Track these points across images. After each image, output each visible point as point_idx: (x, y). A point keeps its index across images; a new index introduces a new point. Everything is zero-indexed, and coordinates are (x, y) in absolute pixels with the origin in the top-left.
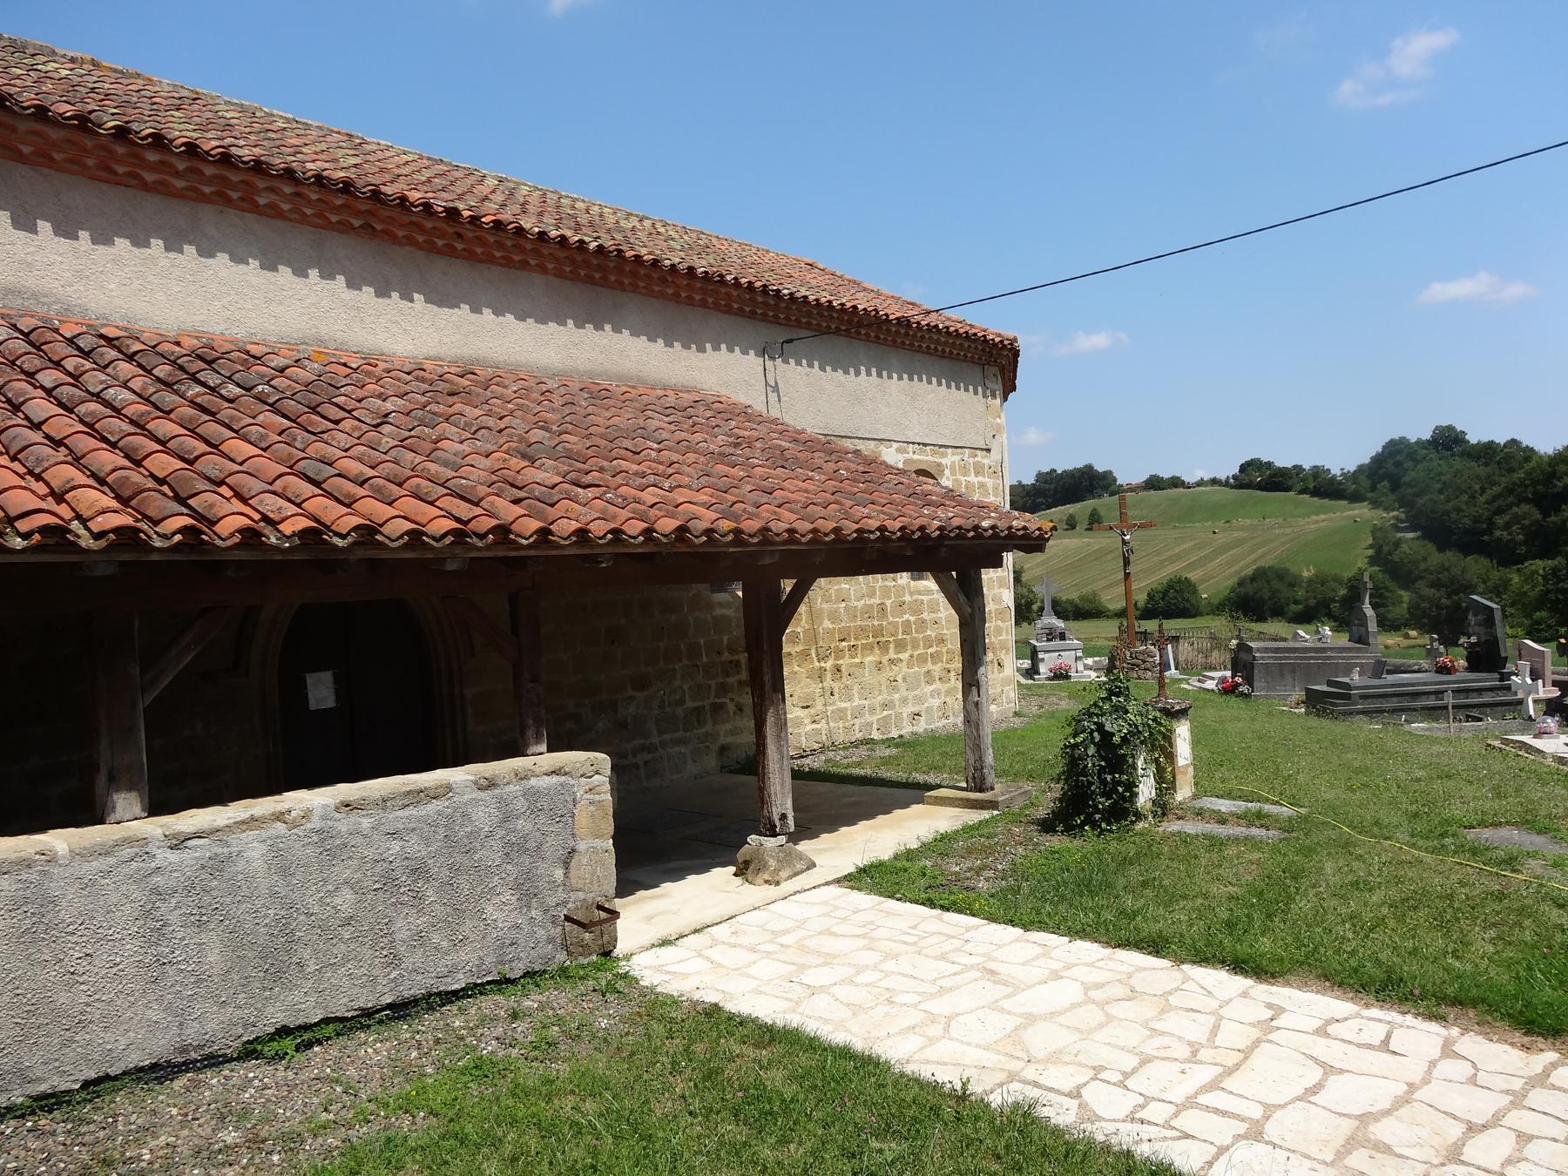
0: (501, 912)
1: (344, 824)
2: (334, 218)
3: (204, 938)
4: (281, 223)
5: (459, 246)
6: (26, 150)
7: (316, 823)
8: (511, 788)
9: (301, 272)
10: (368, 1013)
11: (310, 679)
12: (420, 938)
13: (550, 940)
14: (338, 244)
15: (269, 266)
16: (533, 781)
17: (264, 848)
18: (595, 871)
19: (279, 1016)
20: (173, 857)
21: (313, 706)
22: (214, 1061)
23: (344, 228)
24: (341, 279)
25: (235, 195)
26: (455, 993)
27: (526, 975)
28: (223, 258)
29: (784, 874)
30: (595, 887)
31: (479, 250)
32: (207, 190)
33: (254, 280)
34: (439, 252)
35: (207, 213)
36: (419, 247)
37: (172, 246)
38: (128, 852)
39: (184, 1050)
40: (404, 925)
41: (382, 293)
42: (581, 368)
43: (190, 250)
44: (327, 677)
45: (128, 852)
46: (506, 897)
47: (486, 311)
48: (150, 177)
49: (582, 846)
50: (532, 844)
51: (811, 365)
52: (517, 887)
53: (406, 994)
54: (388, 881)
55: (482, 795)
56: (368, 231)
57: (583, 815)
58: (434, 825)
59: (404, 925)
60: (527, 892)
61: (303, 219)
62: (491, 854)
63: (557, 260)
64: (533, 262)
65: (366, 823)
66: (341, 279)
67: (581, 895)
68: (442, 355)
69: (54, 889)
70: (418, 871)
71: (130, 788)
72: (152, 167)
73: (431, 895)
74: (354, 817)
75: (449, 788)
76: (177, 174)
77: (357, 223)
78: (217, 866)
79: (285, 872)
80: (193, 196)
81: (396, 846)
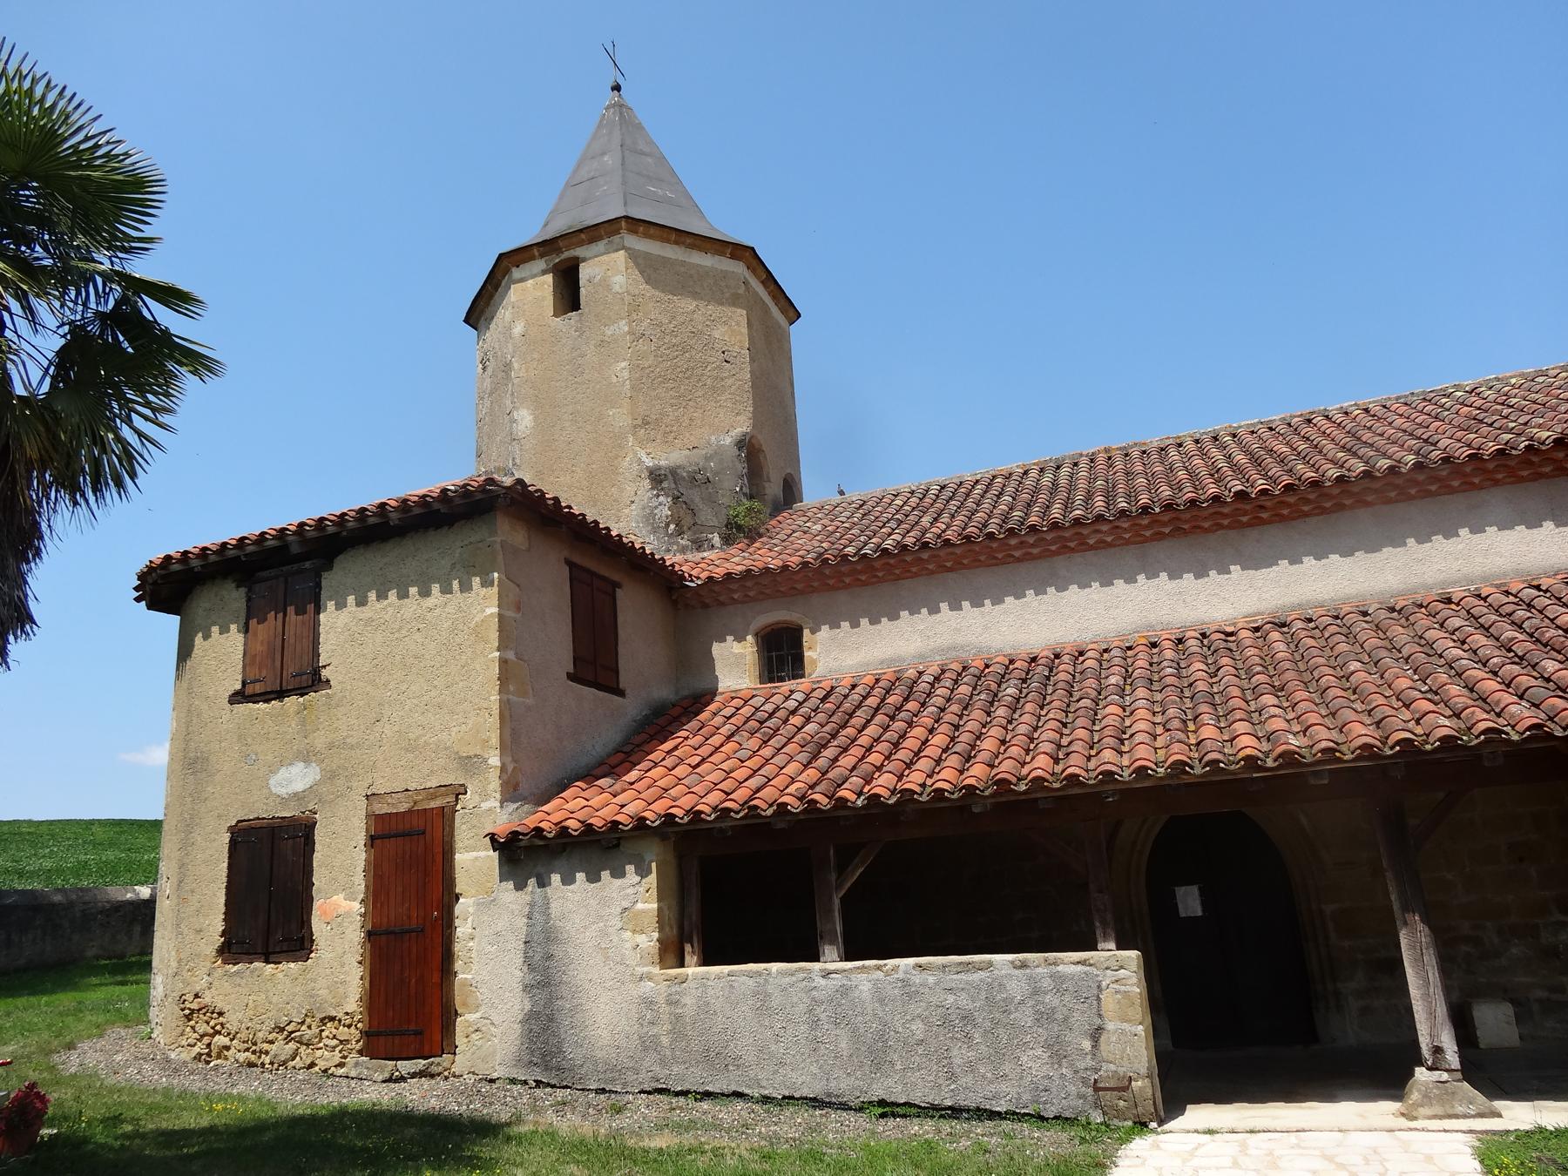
0: (1035, 1062)
1: (917, 978)
2: (1148, 533)
3: (838, 1032)
4: (1113, 550)
5: (1265, 515)
6: (948, 564)
7: (901, 975)
8: (1040, 970)
9: (1131, 580)
10: (935, 1108)
11: (1181, 891)
12: (971, 1067)
13: (1081, 1096)
14: (1158, 550)
15: (1107, 583)
16: (1060, 968)
17: (869, 985)
18: (1124, 1050)
19: (877, 1092)
20: (823, 982)
21: (1183, 914)
22: (845, 1107)
23: (1159, 536)
24: (1164, 575)
25: (1072, 545)
26: (999, 1114)
27: (1056, 1118)
28: (1074, 588)
29: (1423, 1111)
30: (1125, 1062)
31: (1285, 512)
32: (1053, 548)
33: (1095, 596)
34: (1249, 525)
35: (1060, 562)
36: (1229, 527)
37: (1040, 591)
38: (802, 975)
39: (829, 1095)
40: (960, 1055)
41: (1199, 575)
42: (1430, 581)
43: (1051, 590)
44: (1194, 890)
45: (802, 975)
46: (1039, 1052)
47: (1305, 559)
48: (1017, 554)
49: (1110, 1026)
50: (1059, 1016)
51: (855, 625)
52: (1048, 1046)
53: (962, 1103)
54: (946, 1022)
55: (1017, 972)
56: (1178, 532)
57: (1109, 1001)
58: (978, 988)
59: (960, 1055)
60: (1058, 1054)
61: (1128, 542)
62: (1025, 1017)
63: (1376, 491)
64: (1347, 502)
65: (931, 980)
66: (1164, 575)
67: (1112, 1067)
68: (1262, 609)
69: (770, 989)
70: (967, 1018)
71: (831, 943)
72: (1016, 548)
73: (978, 1038)
74: (925, 975)
75: (990, 964)
76: (1033, 546)
77: (1167, 530)
78: (844, 991)
79: (881, 1001)
80: (1047, 554)
81: (951, 999)
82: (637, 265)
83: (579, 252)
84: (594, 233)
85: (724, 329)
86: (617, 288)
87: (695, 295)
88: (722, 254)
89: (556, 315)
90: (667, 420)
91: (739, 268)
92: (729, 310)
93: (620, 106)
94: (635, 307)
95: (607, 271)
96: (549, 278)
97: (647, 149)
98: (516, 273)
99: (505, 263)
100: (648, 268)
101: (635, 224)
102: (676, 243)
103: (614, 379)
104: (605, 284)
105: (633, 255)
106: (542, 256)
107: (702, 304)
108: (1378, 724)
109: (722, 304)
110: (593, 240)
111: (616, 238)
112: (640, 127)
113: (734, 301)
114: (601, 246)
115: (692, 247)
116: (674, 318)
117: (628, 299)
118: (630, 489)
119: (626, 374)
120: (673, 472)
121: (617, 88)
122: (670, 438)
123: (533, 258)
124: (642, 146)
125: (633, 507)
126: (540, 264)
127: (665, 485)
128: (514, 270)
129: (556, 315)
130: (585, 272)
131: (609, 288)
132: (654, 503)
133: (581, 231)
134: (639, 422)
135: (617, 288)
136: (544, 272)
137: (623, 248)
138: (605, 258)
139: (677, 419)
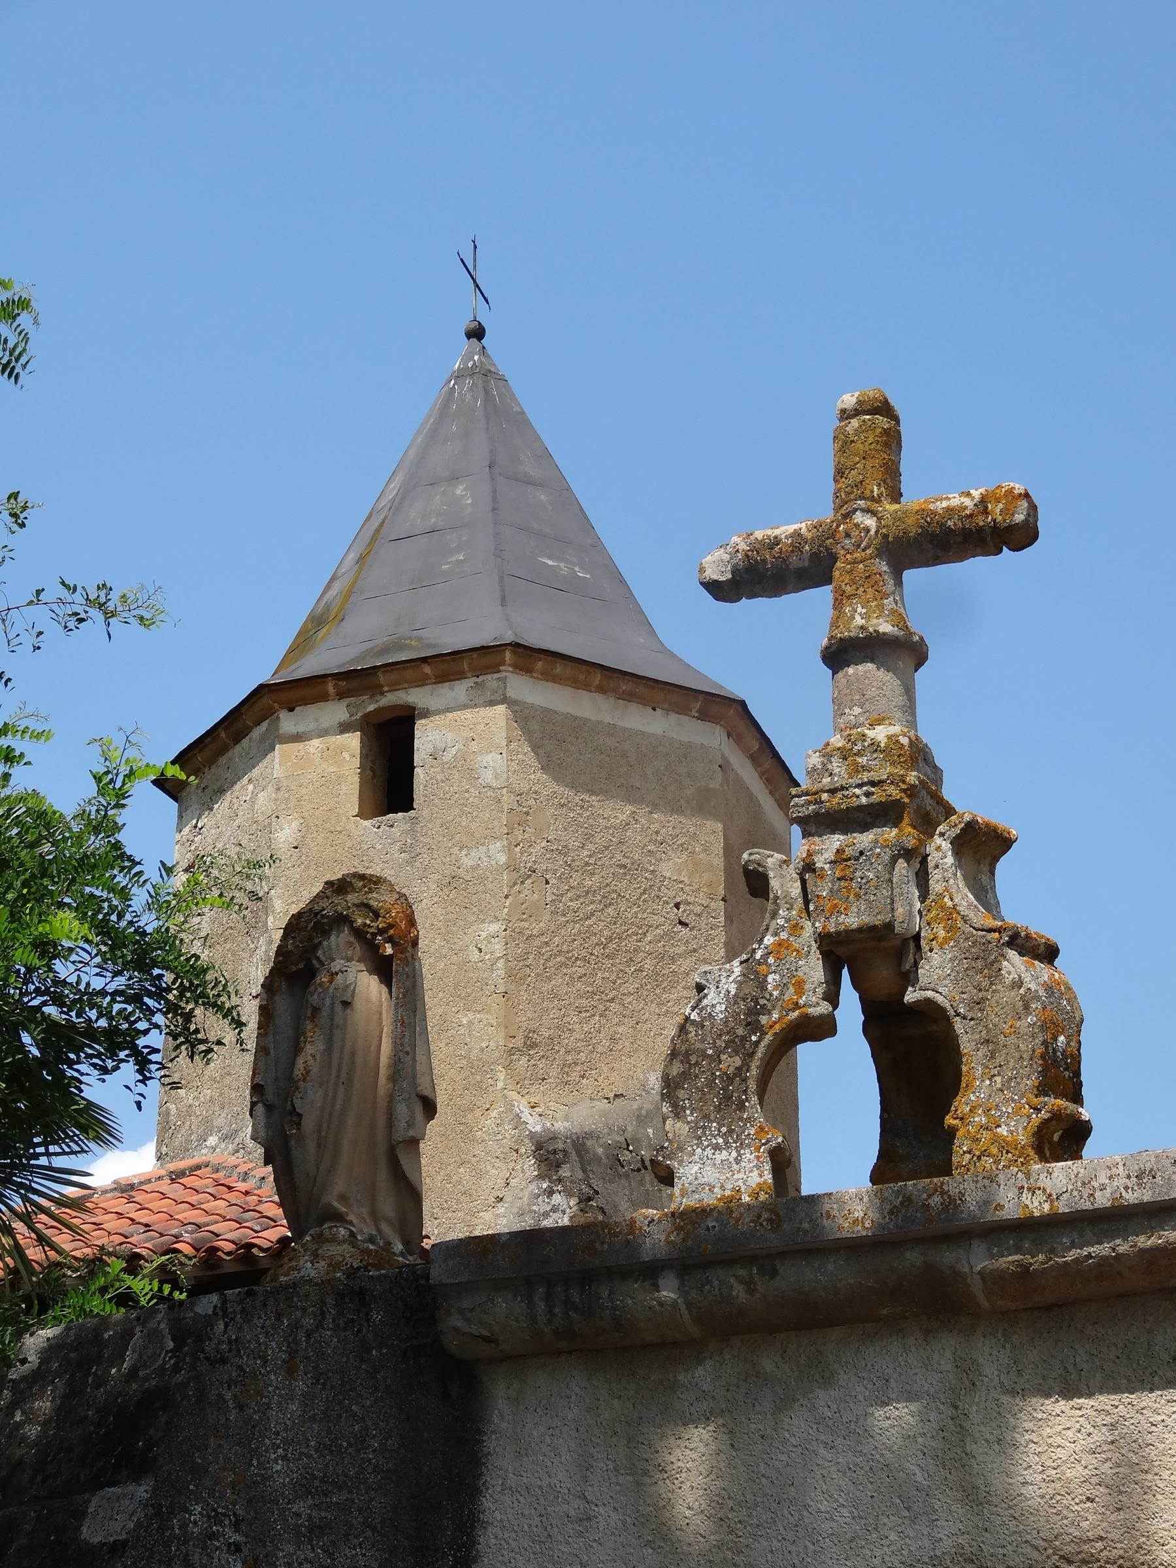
82: (528, 733)
83: (415, 697)
84: (449, 666)
85: (680, 859)
86: (488, 777)
87: (631, 795)
88: (683, 710)
89: (362, 814)
90: (569, 1040)
91: (711, 738)
92: (690, 824)
93: (485, 376)
94: (520, 818)
95: (466, 741)
96: (353, 741)
97: (535, 472)
98: (288, 722)
99: (266, 700)
100: (544, 736)
101: (529, 657)
102: (601, 690)
103: (475, 956)
104: (466, 767)
105: (522, 715)
106: (341, 695)
107: (642, 811)
108: (1113, 1426)
109: (679, 810)
110: (444, 677)
111: (491, 680)
112: (521, 421)
113: (702, 805)
114: (460, 690)
115: (630, 697)
116: (589, 837)
117: (508, 800)
118: (495, 1173)
119: (498, 947)
120: (579, 1145)
121: (477, 333)
122: (574, 1076)
123: (324, 697)
124: (530, 468)
125: (501, 1209)
126: (337, 712)
127: (565, 1172)
128: (283, 715)
129: (362, 814)
130: (428, 738)
131: (472, 774)
132: (543, 1205)
133: (424, 660)
134: (519, 1042)
135: (488, 777)
136: (344, 728)
137: (504, 700)
138: (467, 715)
139: (587, 1039)
